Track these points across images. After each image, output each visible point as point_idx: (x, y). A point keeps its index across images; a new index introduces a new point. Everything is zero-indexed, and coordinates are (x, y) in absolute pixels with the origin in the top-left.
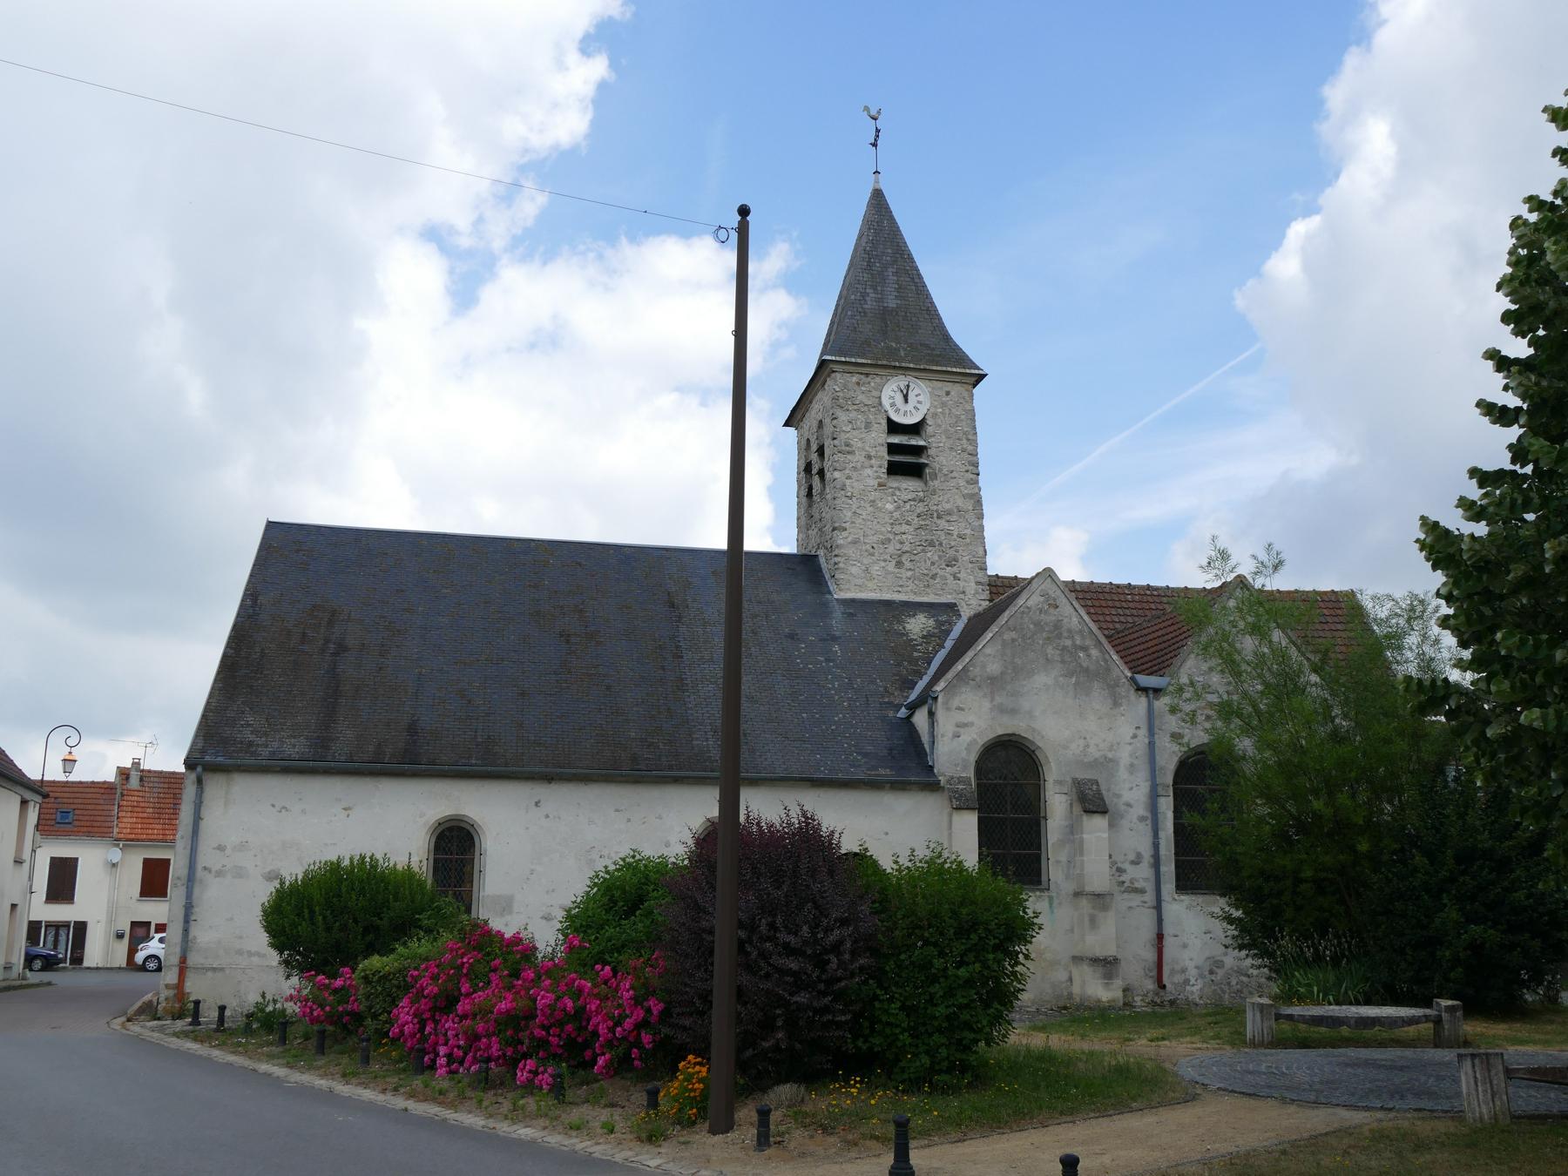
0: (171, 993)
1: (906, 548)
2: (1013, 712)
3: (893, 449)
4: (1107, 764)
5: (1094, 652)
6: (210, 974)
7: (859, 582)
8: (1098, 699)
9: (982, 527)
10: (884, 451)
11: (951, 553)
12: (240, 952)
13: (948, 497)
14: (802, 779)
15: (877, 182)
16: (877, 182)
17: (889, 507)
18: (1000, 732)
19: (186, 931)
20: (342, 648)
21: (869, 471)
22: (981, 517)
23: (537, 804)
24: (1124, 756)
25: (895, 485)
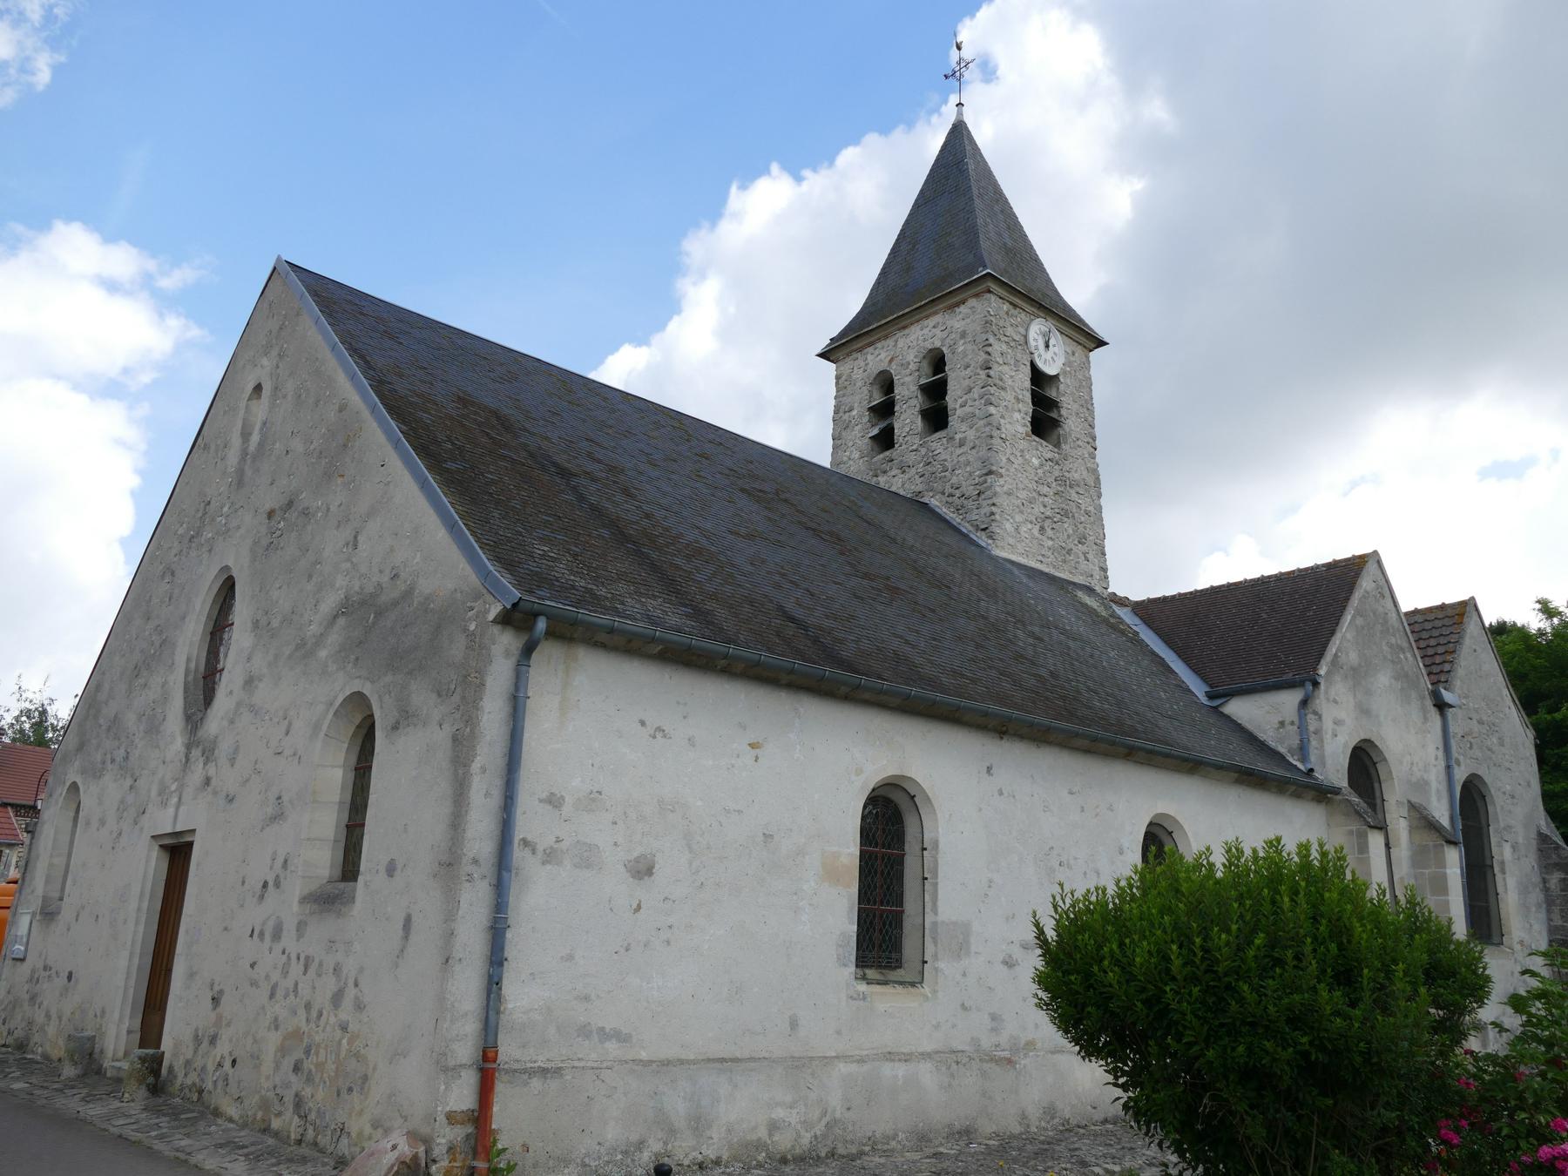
0: (458, 1133)
6: (536, 1083)
9: (1099, 509)
12: (584, 1031)
14: (1219, 767)
15: (960, 113)
16: (960, 113)
17: (1035, 462)
19: (493, 985)
21: (1017, 416)
22: (1099, 496)
23: (989, 769)
24: (1434, 785)
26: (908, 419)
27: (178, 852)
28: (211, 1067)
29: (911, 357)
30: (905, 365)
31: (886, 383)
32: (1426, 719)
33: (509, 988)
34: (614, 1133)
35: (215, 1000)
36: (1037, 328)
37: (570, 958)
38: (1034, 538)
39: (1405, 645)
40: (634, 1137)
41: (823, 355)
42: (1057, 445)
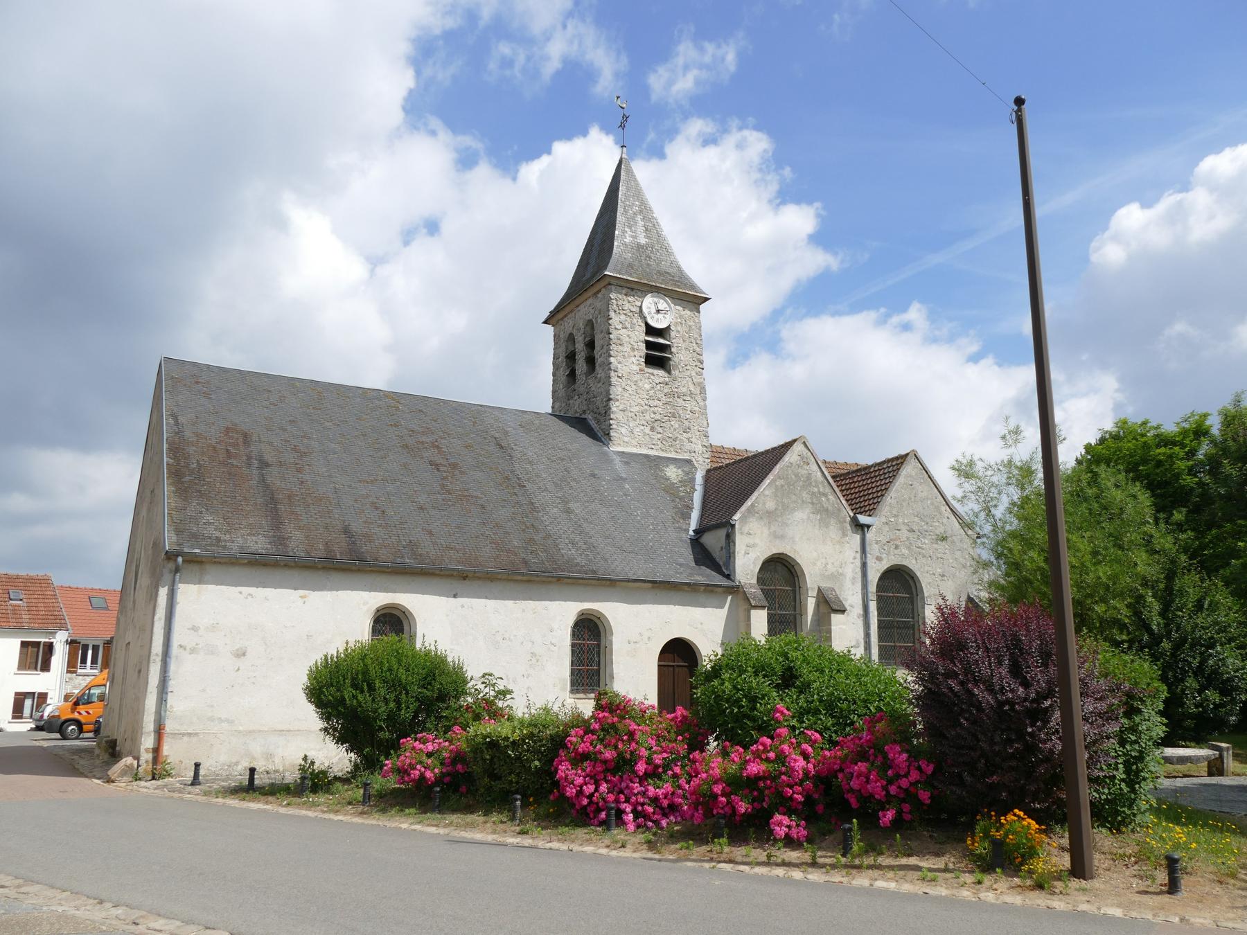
1: (658, 417)
2: (782, 537)
3: (649, 345)
4: (837, 576)
5: (831, 497)
6: (186, 739)
7: (626, 439)
8: (834, 531)
10: (643, 346)
11: (686, 423)
12: (211, 719)
13: (685, 385)
17: (647, 386)
18: (775, 552)
20: (264, 464)
21: (634, 360)
25: (650, 370)
26: (581, 366)
29: (581, 325)
30: (579, 330)
31: (571, 338)
32: (844, 535)
33: (171, 699)
34: (224, 758)
36: (649, 303)
37: (204, 690)
38: (645, 434)
39: (828, 490)
40: (234, 760)
41: (545, 322)
42: (669, 372)
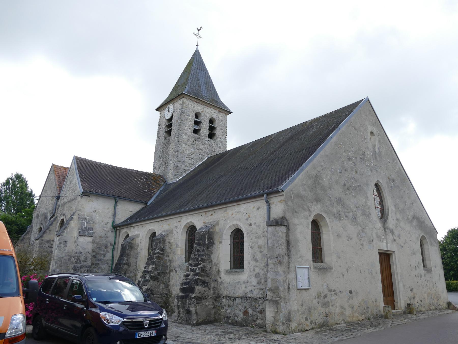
27: (385, 257)
28: (416, 303)
35: (412, 290)
